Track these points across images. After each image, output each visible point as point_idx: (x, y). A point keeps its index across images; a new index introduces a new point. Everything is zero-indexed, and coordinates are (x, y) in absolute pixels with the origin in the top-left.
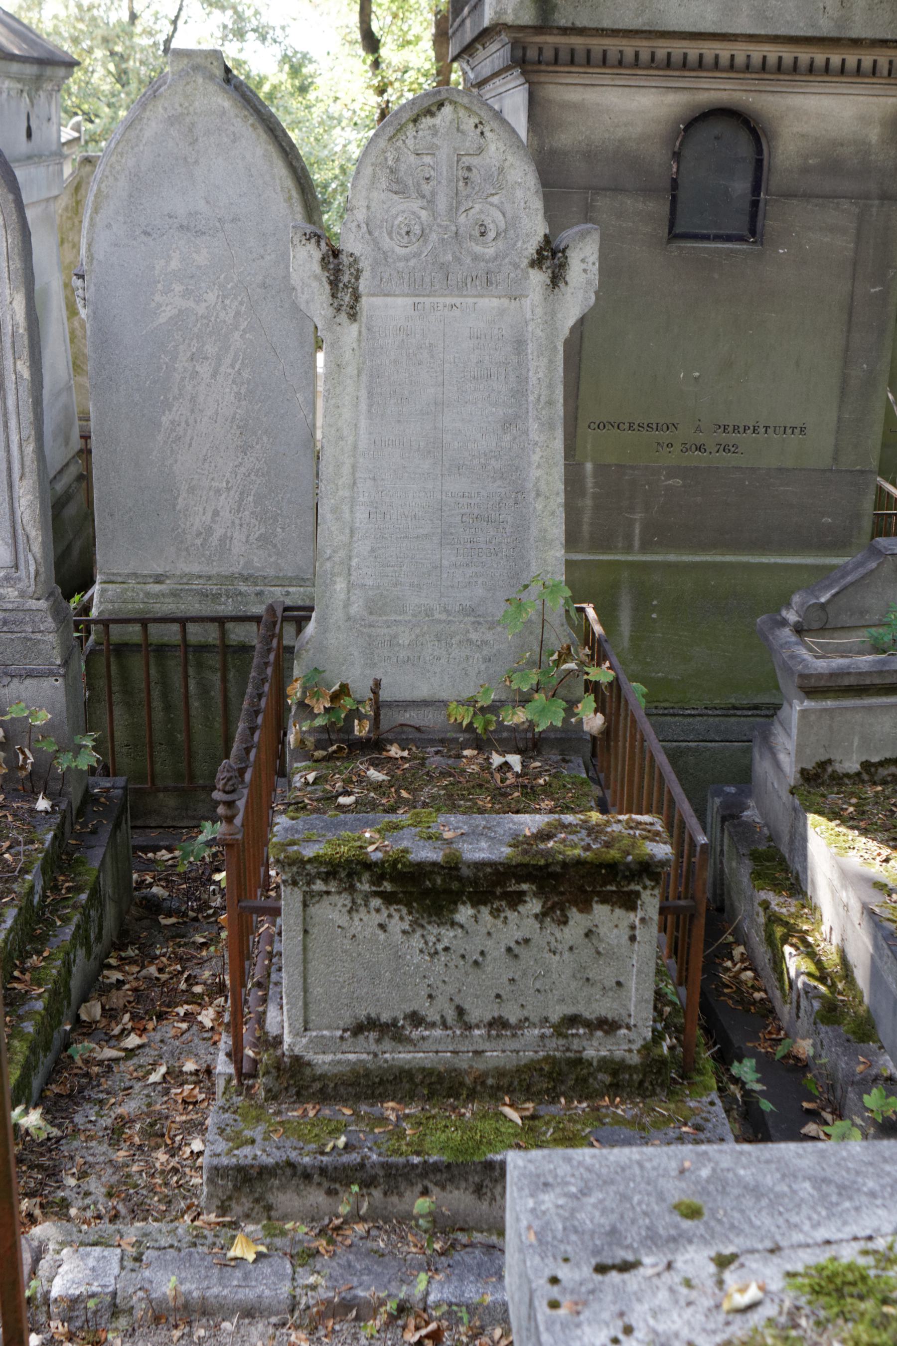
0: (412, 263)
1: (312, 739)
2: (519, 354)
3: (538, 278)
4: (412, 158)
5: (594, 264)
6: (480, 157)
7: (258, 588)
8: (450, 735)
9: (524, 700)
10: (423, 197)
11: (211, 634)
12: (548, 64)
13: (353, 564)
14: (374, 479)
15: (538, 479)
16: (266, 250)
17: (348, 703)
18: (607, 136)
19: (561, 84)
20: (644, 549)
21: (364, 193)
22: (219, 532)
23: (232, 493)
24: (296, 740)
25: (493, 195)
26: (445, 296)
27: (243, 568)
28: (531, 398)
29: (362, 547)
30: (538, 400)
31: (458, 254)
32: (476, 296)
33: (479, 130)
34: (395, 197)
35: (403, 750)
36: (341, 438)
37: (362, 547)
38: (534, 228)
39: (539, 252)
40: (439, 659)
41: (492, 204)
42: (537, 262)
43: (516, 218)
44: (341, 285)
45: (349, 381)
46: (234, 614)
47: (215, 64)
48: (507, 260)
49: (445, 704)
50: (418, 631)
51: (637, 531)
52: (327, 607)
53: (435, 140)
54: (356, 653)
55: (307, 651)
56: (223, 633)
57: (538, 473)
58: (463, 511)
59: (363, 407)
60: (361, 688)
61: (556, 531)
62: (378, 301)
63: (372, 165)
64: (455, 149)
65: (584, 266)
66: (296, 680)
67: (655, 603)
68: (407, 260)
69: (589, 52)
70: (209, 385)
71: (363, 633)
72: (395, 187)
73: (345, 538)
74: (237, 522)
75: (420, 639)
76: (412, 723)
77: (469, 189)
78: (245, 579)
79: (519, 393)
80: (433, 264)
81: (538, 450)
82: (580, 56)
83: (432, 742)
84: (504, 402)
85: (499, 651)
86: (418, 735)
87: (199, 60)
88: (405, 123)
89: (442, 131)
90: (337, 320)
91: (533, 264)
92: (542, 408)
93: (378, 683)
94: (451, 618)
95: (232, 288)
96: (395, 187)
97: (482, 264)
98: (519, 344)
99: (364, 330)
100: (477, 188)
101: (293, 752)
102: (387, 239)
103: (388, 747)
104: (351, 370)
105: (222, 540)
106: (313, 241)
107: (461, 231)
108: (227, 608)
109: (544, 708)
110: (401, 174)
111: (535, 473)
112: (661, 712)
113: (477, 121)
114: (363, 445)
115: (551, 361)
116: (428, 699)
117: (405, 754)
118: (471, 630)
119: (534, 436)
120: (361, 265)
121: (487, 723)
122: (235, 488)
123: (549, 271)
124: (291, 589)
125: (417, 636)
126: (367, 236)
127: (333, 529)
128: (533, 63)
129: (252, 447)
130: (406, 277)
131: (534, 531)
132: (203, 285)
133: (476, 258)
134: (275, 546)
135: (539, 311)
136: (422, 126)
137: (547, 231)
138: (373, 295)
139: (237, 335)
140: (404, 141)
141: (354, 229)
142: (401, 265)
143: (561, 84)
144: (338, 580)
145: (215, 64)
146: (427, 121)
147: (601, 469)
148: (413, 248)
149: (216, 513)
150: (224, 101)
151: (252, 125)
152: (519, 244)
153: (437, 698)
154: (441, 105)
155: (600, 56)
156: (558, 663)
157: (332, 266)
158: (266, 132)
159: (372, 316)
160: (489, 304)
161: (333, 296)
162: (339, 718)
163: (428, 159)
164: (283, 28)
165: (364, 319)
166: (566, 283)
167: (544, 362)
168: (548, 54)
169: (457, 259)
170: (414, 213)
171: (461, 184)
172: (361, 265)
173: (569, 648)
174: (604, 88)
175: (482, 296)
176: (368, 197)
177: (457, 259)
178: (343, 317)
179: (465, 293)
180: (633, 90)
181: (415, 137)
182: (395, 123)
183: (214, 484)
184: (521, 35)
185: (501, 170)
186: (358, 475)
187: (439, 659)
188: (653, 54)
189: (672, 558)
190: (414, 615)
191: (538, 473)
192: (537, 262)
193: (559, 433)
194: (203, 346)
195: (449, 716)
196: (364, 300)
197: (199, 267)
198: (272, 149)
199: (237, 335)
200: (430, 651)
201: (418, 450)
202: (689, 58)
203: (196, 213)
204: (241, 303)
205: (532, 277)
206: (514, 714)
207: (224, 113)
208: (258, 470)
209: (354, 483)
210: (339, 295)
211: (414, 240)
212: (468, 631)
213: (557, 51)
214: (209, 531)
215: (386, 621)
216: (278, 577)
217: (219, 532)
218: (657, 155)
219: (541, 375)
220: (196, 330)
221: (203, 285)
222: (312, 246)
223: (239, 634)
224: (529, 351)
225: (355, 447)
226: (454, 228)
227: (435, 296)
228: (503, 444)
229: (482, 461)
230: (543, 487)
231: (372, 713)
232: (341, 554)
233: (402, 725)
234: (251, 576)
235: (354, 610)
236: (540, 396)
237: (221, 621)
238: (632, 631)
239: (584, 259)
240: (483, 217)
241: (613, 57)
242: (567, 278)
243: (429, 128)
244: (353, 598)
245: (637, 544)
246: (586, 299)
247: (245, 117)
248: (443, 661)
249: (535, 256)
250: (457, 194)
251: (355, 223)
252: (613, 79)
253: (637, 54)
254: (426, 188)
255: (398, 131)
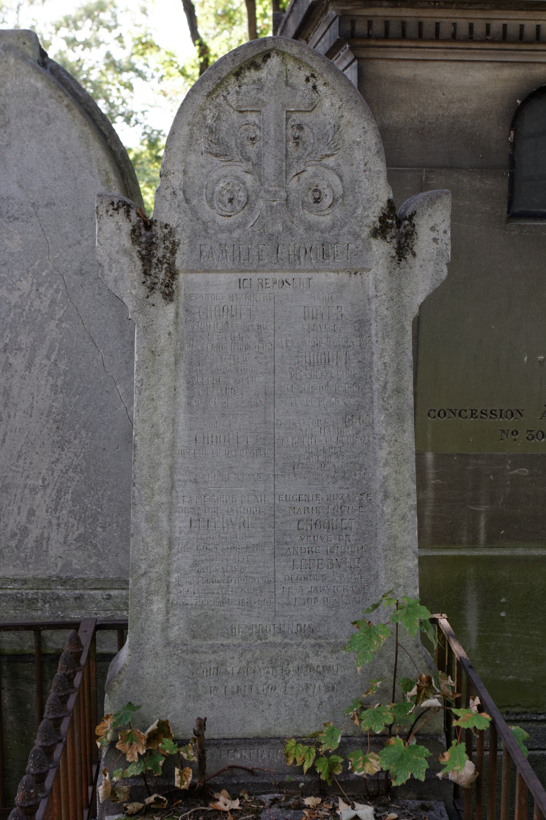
0: (236, 234)
1: (125, 788)
2: (361, 336)
3: (382, 249)
4: (235, 116)
5: (445, 232)
6: (312, 114)
7: (77, 592)
8: (288, 778)
9: (378, 742)
10: (248, 159)
11: (27, 642)
12: (378, 38)
13: (173, 580)
14: (196, 482)
15: (385, 478)
16: (82, 236)
17: (167, 746)
18: (440, 112)
19: (392, 60)
20: (491, 542)
21: (180, 156)
22: (35, 532)
23: (49, 491)
24: (105, 792)
25: (328, 156)
26: (275, 271)
27: (61, 571)
28: (376, 386)
29: (183, 560)
30: (385, 387)
31: (289, 223)
32: (310, 271)
33: (310, 84)
34: (216, 160)
35: (234, 799)
36: (157, 435)
37: (183, 560)
38: (377, 193)
39: (382, 220)
40: (274, 688)
41: (327, 167)
42: (380, 231)
43: (355, 182)
44: (155, 260)
45: (165, 370)
46: (51, 620)
47: (28, 44)
48: (345, 229)
49: (282, 741)
50: (249, 656)
51: (482, 524)
52: (143, 630)
53: (260, 96)
54: (177, 684)
55: (120, 683)
56: (40, 641)
57: (386, 471)
58: (299, 517)
59: (182, 399)
60: (184, 727)
61: (408, 538)
62: (198, 278)
63: (189, 124)
64: (284, 106)
65: (434, 235)
66: (108, 717)
67: (503, 600)
68: (231, 231)
69: (420, 24)
70: (23, 378)
71: (184, 661)
72: (216, 149)
73: (162, 551)
74: (55, 521)
75: (252, 665)
76: (244, 765)
77: (300, 150)
78: (64, 582)
79: (362, 381)
80: (261, 235)
81: (385, 444)
82: (412, 30)
83: (267, 788)
84: (345, 391)
85: (344, 678)
86: (251, 779)
87: (11, 40)
88: (227, 77)
89: (269, 85)
90: (150, 300)
91: (375, 233)
92: (390, 397)
93: (202, 724)
94: (287, 640)
95: (47, 275)
96: (216, 149)
97: (318, 234)
98: (361, 324)
99: (181, 312)
100: (309, 149)
101: (102, 805)
102: (207, 208)
103: (216, 796)
104: (168, 357)
105: (38, 541)
106: (122, 211)
107: (291, 198)
108: (43, 614)
109: (402, 756)
110: (222, 134)
111: (382, 472)
112: (513, 718)
113: (308, 74)
114: (181, 444)
115: (398, 343)
116: (262, 736)
117: (236, 804)
118: (311, 654)
119: (380, 429)
120: (177, 237)
121: (332, 766)
122: (52, 486)
123: (394, 241)
124: (113, 593)
125: (248, 663)
126: (184, 204)
127: (148, 540)
128: (362, 38)
129: (69, 442)
130: (230, 250)
131: (383, 539)
132: (16, 273)
133: (310, 227)
134: (95, 547)
135: (384, 286)
136: (246, 80)
137: (391, 196)
138: (192, 271)
139: (52, 324)
140: (225, 98)
141: (169, 197)
142: (223, 236)
143: (392, 60)
144: (155, 598)
145: (28, 44)
146: (251, 75)
147: (440, 458)
148: (237, 218)
149: (32, 513)
150: (38, 83)
151: (67, 106)
152: (359, 211)
153: (273, 733)
154: (267, 56)
155: (433, 29)
156: (417, 699)
157: (143, 239)
158: (81, 113)
159: (191, 295)
160: (326, 279)
161: (146, 273)
162: (156, 766)
163: (252, 117)
164: (143, 112)
165: (182, 299)
166: (414, 255)
167: (390, 344)
168: (378, 28)
169: (289, 230)
170: (237, 178)
171: (291, 144)
172: (177, 237)
173: (429, 680)
174: (437, 63)
175: (317, 271)
176: (184, 161)
177: (289, 230)
178: (157, 298)
179: (297, 267)
180: (467, 65)
181: (238, 93)
182: (215, 76)
183: (30, 482)
184: (349, 8)
185: (337, 128)
186: (177, 477)
187: (274, 688)
188: (488, 26)
189: (520, 552)
190: (244, 638)
191: (386, 471)
192: (380, 231)
193: (409, 425)
194: (17, 336)
195: (287, 755)
196: (181, 277)
197: (12, 254)
198: (88, 130)
199: (52, 324)
200: (263, 679)
201: (247, 447)
202: (526, 29)
203: (9, 198)
204: (57, 291)
205: (374, 248)
206: (365, 761)
207: (37, 94)
208: (76, 467)
209: (173, 487)
210: (153, 272)
211: (238, 208)
212: (307, 656)
213: (387, 24)
214: (25, 531)
215: (212, 646)
216: (98, 580)
217: (35, 532)
218: (496, 133)
219: (387, 359)
220: (9, 320)
221: (16, 273)
222: (120, 217)
223: (57, 641)
224: (373, 332)
225: (173, 445)
226: (284, 194)
227: (263, 271)
228: (345, 439)
229: (321, 458)
230: (392, 487)
231: (195, 759)
232: (159, 569)
233: (231, 767)
234: (69, 579)
235: (174, 633)
236: (386, 383)
237: (36, 628)
238: (479, 631)
239: (434, 227)
240: (317, 181)
241: (446, 30)
242: (415, 249)
243: (254, 82)
244: (173, 620)
245: (482, 537)
246: (437, 272)
247: (60, 97)
248: (279, 691)
249: (378, 224)
250: (286, 156)
251: (170, 190)
252: (446, 54)
253: (471, 26)
254: (251, 150)
255: (218, 85)
